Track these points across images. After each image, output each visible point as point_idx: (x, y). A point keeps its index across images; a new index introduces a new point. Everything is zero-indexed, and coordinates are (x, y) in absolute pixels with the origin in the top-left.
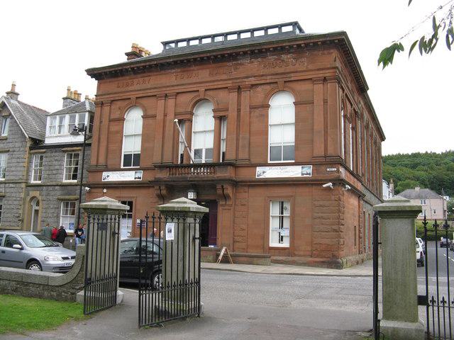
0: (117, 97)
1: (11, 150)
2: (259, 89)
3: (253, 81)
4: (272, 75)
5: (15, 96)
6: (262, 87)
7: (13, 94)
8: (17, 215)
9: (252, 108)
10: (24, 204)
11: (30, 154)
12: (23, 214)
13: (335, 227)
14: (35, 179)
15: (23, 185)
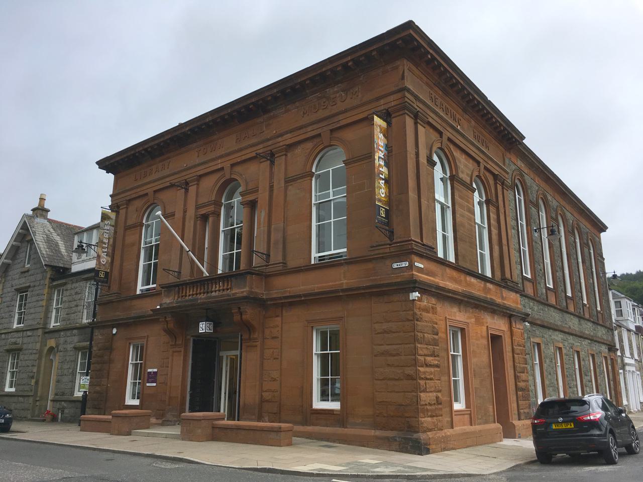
0: (201, 170)
1: (32, 285)
2: (299, 150)
3: (289, 139)
4: (291, 131)
5: (44, 213)
6: (302, 146)
7: (41, 211)
8: (31, 374)
9: (289, 181)
10: (40, 359)
11: (52, 288)
12: (38, 371)
13: (409, 371)
14: (324, 396)
15: (40, 332)
